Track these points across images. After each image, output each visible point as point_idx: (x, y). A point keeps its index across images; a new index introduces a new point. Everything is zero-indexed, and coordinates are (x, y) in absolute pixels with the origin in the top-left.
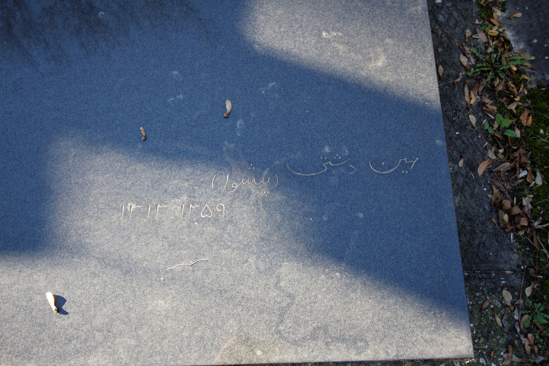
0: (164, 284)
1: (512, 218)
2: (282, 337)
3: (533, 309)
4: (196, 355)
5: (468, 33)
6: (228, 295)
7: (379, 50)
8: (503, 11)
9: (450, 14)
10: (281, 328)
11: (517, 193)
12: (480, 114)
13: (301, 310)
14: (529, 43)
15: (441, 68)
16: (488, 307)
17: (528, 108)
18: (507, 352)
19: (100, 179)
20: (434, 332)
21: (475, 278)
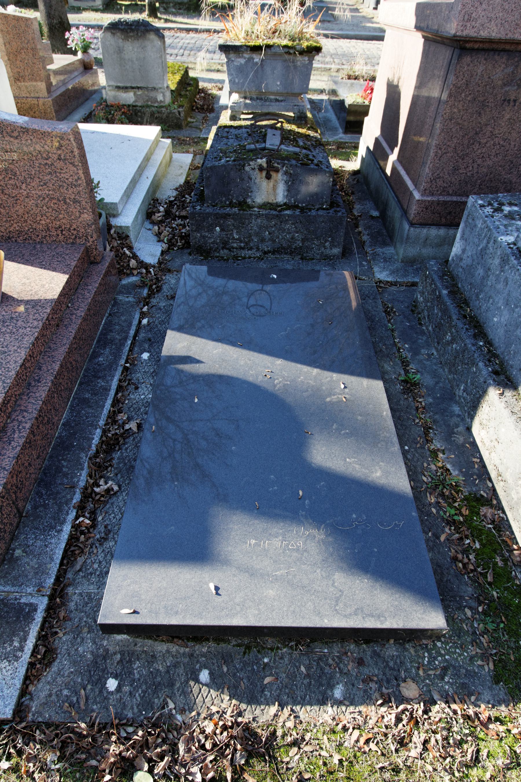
0: (272, 582)
1: (464, 565)
2: (338, 613)
3: (485, 620)
4: (291, 621)
5: (425, 465)
6: (307, 589)
7: (377, 468)
8: (444, 454)
9: (414, 455)
10: (337, 608)
11: (466, 551)
12: (438, 508)
13: (347, 598)
14: (461, 471)
15: (412, 483)
16: (457, 618)
17: (465, 505)
18: (473, 646)
19: (236, 527)
20: (423, 614)
21: (447, 600)
